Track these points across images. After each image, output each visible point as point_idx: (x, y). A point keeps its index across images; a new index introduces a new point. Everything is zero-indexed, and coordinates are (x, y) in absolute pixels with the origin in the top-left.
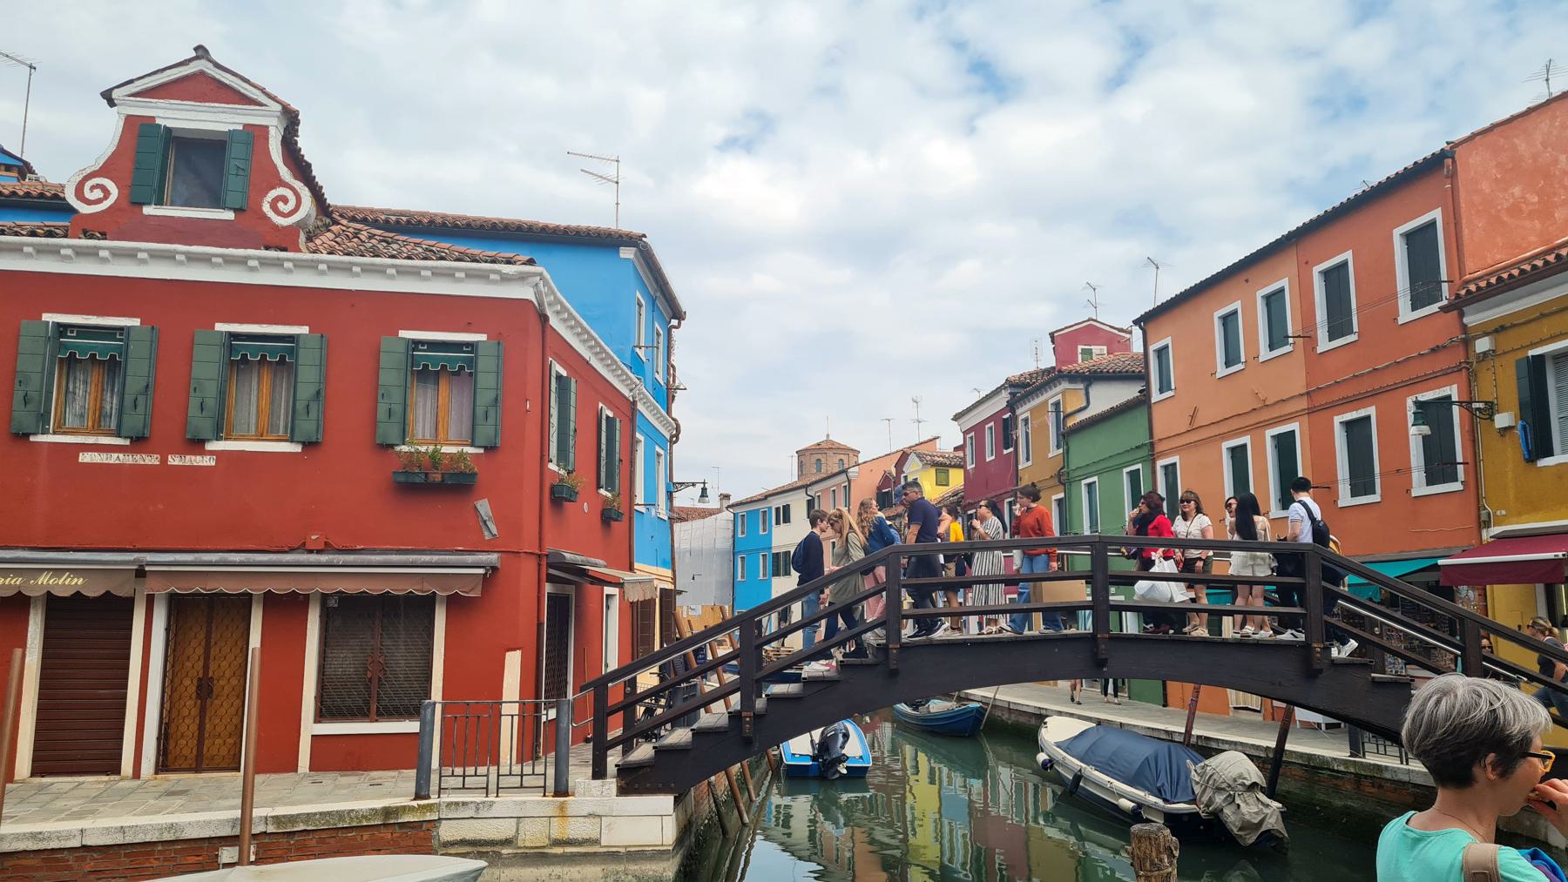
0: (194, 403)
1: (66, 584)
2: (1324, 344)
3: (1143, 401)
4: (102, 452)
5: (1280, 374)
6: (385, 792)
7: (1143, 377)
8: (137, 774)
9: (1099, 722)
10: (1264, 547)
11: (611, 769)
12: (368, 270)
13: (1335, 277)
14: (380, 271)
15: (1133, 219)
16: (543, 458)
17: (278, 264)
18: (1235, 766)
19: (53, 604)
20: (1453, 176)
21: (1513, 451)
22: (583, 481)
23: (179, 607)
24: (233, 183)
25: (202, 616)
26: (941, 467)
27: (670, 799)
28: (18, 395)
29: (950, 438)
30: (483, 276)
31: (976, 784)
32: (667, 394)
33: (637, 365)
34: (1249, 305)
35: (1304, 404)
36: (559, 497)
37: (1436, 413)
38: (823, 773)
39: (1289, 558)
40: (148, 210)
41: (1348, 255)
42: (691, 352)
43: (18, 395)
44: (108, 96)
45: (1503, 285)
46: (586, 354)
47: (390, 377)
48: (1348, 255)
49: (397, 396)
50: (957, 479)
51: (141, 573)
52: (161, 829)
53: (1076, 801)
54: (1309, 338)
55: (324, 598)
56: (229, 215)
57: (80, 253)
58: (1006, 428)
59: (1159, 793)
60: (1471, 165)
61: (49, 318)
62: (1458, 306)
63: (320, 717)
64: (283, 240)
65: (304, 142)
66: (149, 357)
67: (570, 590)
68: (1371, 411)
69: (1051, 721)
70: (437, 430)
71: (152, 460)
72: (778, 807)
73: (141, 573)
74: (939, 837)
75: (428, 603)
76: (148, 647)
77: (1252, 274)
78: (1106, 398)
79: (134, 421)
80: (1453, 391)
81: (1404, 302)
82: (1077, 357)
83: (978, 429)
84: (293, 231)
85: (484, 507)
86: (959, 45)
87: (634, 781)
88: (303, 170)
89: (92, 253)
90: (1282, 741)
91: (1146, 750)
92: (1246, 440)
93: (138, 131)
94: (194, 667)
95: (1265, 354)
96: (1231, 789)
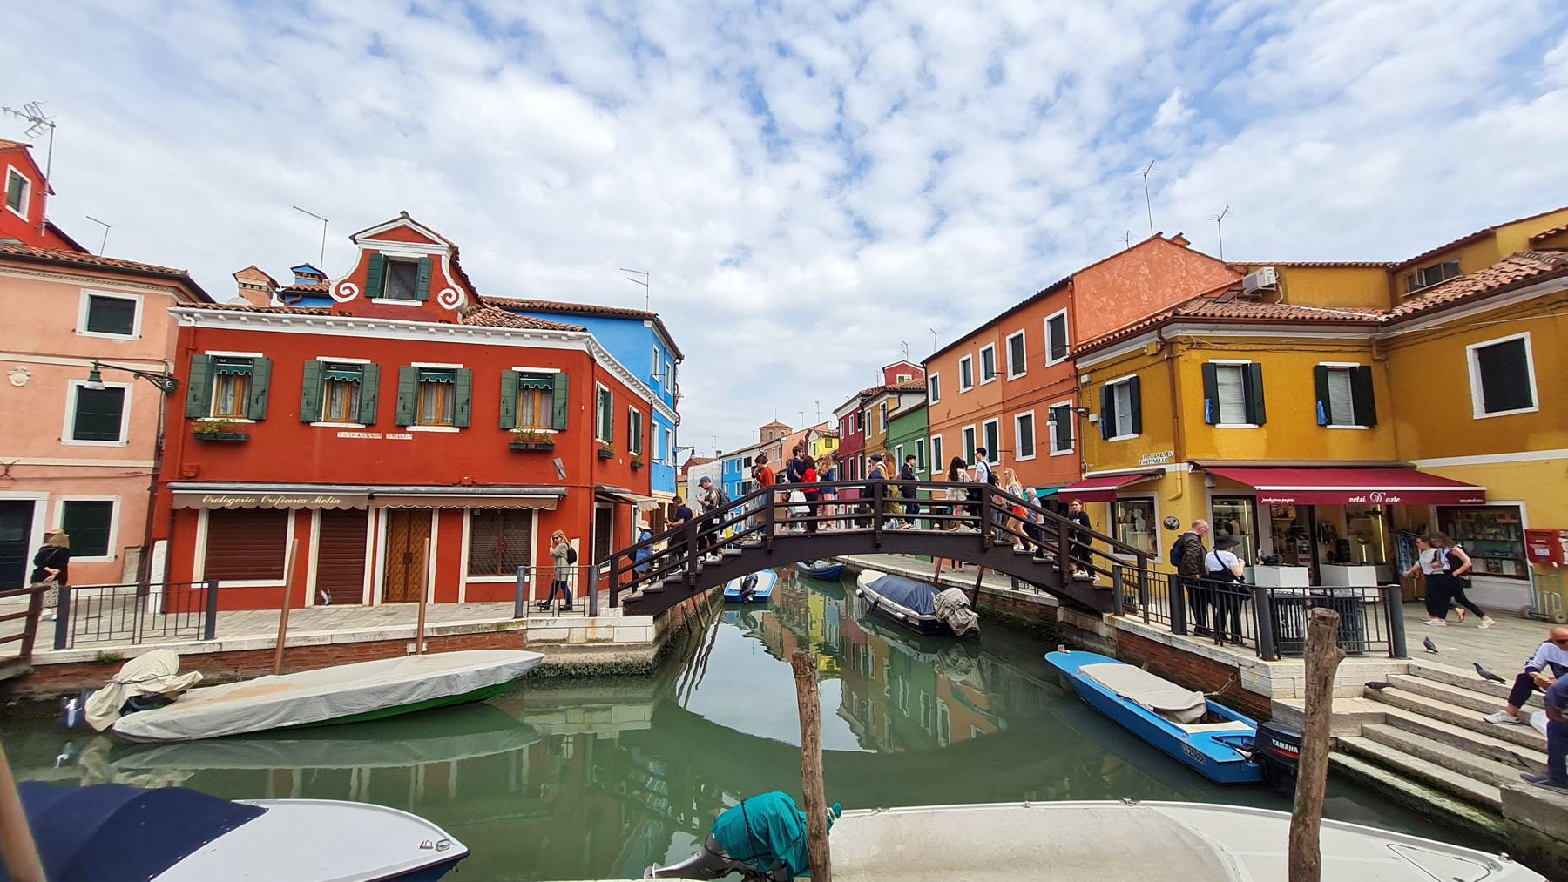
0: (400, 406)
1: (331, 503)
2: (1011, 377)
3: (925, 405)
4: (351, 431)
5: (988, 390)
6: (497, 614)
7: (925, 392)
8: (371, 604)
9: (889, 572)
10: (962, 485)
11: (620, 602)
12: (495, 333)
13: (1017, 342)
14: (502, 334)
15: (941, 306)
16: (594, 435)
17: (446, 330)
18: (955, 595)
19: (325, 515)
20: (1072, 291)
21: (1097, 433)
22: (615, 449)
23: (393, 515)
24: (422, 286)
25: (408, 521)
26: (828, 438)
27: (651, 617)
28: (304, 401)
29: (833, 424)
30: (558, 337)
31: (842, 602)
32: (674, 400)
33: (654, 385)
34: (975, 355)
35: (1000, 408)
36: (603, 457)
37: (1061, 415)
38: (746, 602)
39: (975, 491)
40: (374, 301)
41: (1022, 331)
42: (687, 379)
43: (304, 401)
44: (353, 238)
45: (1094, 349)
46: (621, 379)
47: (507, 392)
48: (1022, 331)
49: (511, 401)
50: (835, 444)
51: (371, 497)
52: (375, 634)
53: (876, 614)
54: (1004, 373)
55: (472, 511)
56: (420, 304)
57: (337, 324)
58: (859, 418)
59: (917, 610)
60: (1080, 284)
61: (321, 359)
62: (1073, 358)
63: (471, 573)
64: (449, 317)
65: (461, 263)
66: (380, 381)
67: (611, 506)
68: (1032, 412)
69: (864, 572)
70: (533, 421)
71: (378, 436)
72: (1235, 515)
73: (371, 497)
74: (823, 633)
75: (528, 514)
76: (377, 536)
77: (977, 339)
78: (909, 402)
79: (368, 415)
80: (1070, 403)
81: (1049, 355)
82: (896, 382)
83: (846, 418)
84: (454, 313)
85: (559, 462)
86: (849, 212)
87: (632, 608)
88: (462, 279)
89: (344, 324)
90: (979, 581)
91: (912, 586)
92: (973, 426)
93: (370, 257)
94: (402, 547)
95: (983, 381)
96: (952, 608)
